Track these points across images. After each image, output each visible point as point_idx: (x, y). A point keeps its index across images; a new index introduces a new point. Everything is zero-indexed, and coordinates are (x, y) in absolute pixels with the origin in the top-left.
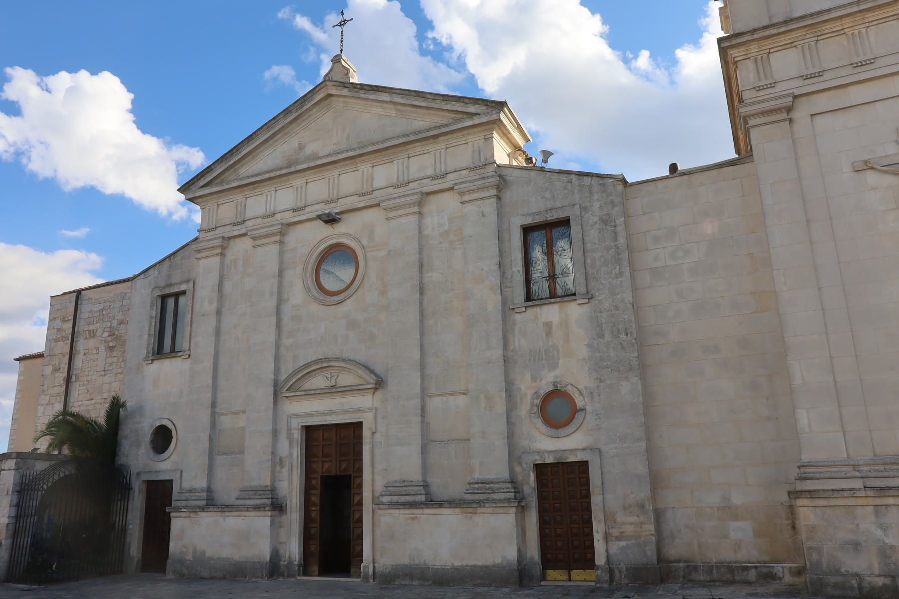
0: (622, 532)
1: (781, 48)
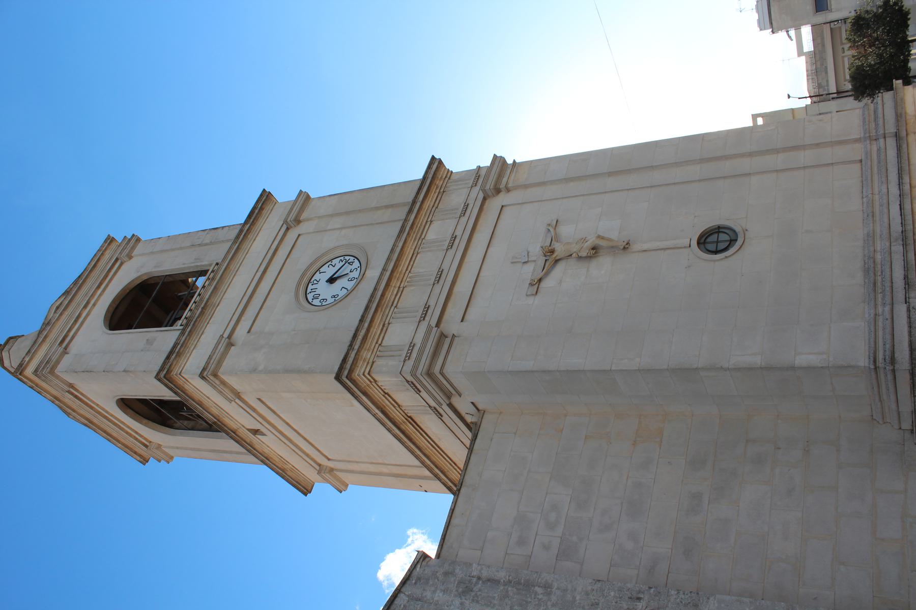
1: (382, 335)
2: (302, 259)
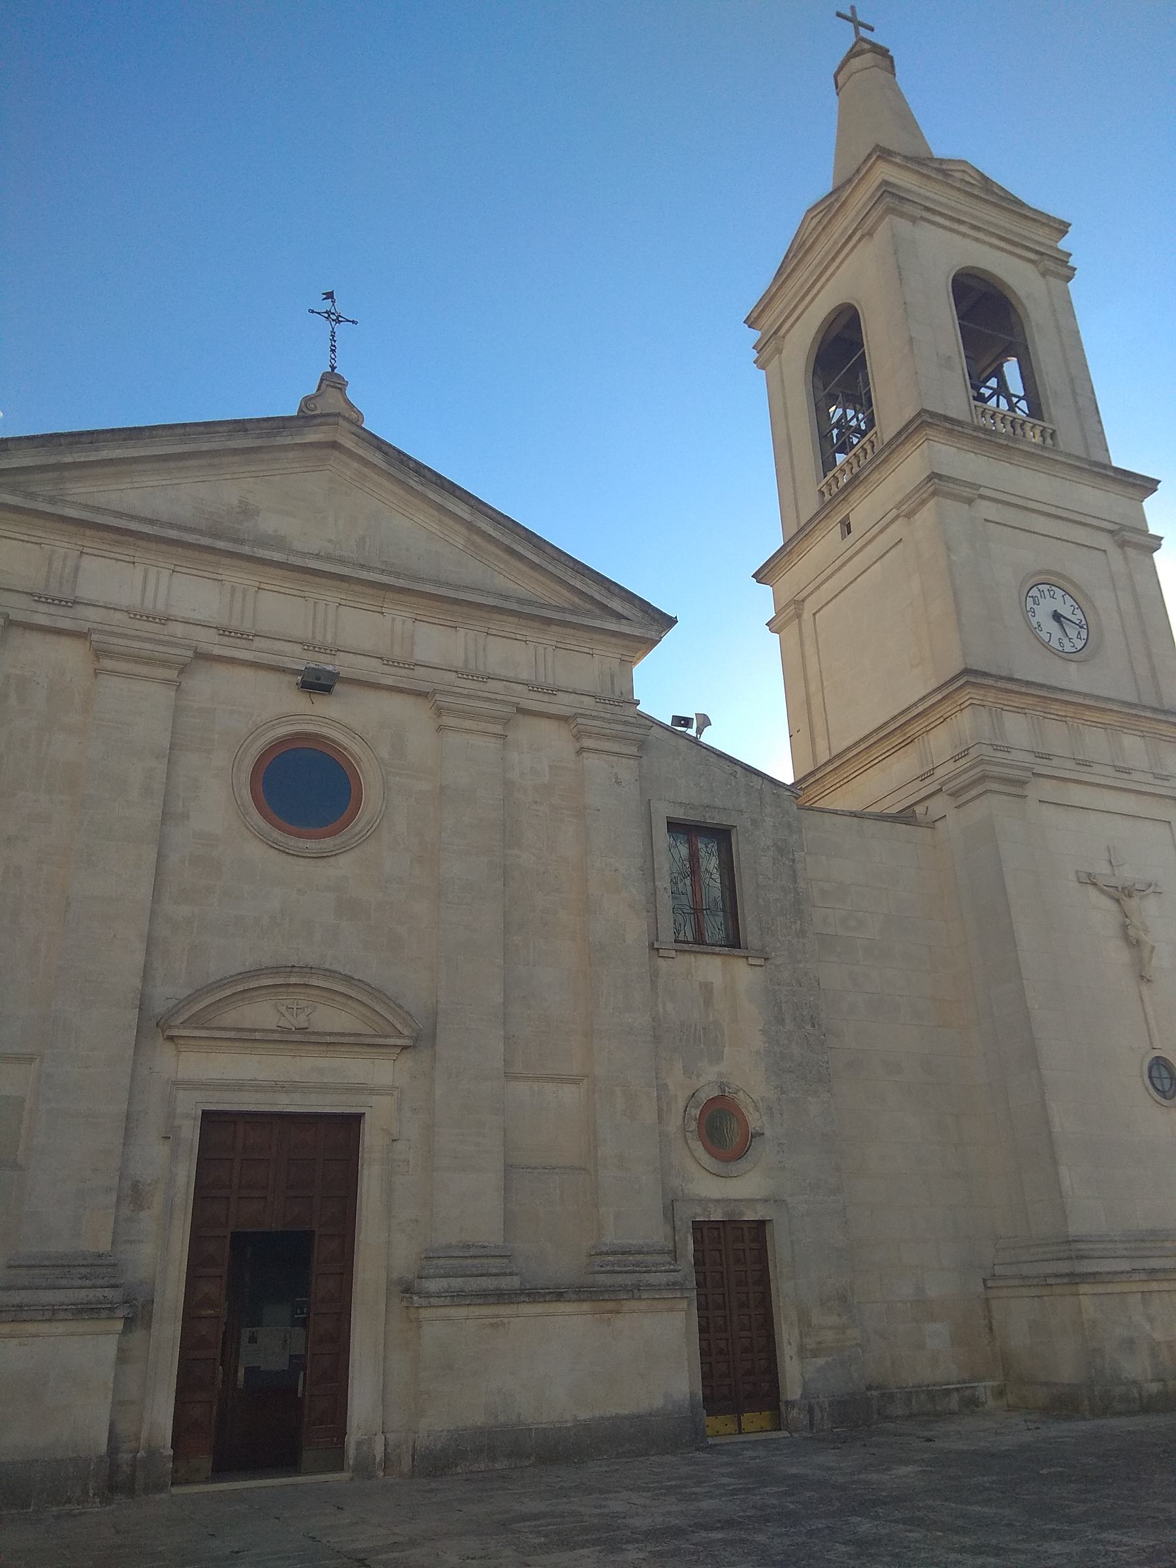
0: (820, 1343)
1: (1013, 709)
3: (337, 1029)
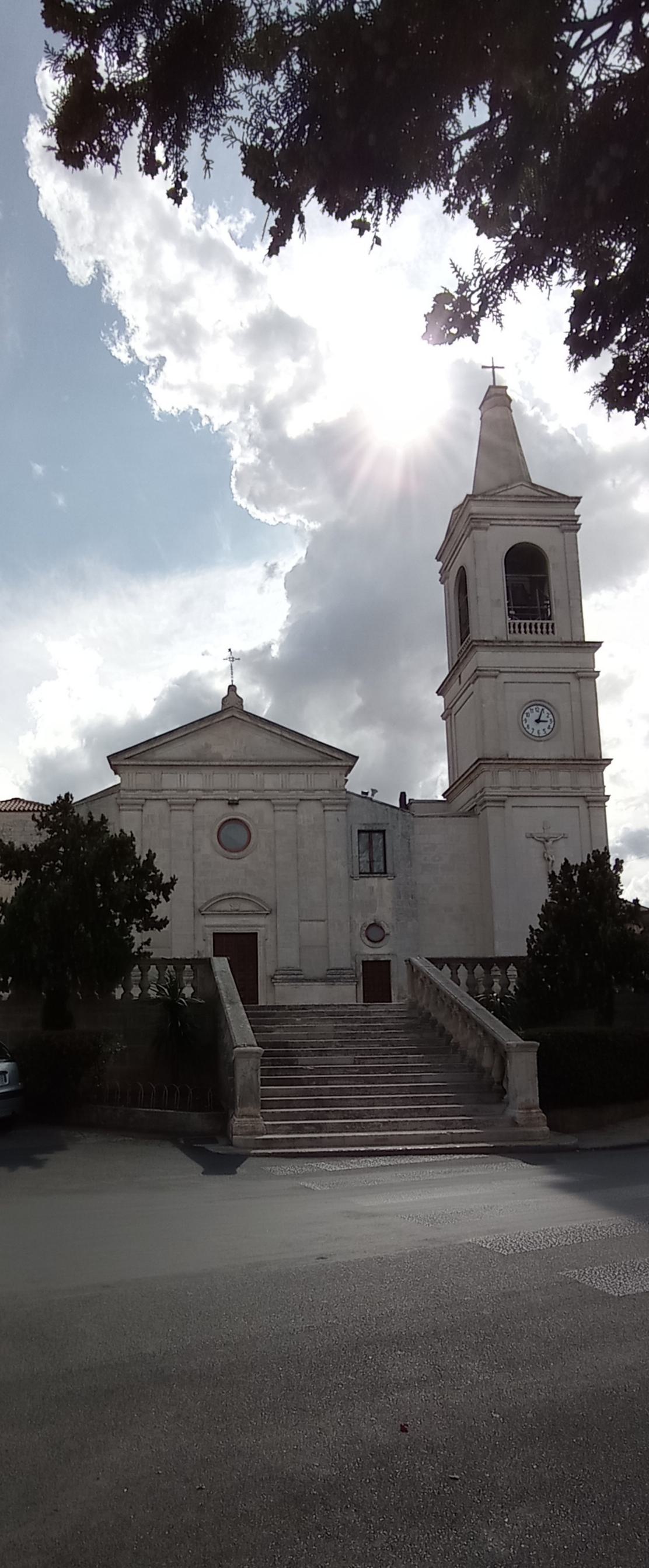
2: (551, 695)
3: (248, 909)
